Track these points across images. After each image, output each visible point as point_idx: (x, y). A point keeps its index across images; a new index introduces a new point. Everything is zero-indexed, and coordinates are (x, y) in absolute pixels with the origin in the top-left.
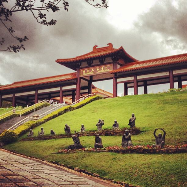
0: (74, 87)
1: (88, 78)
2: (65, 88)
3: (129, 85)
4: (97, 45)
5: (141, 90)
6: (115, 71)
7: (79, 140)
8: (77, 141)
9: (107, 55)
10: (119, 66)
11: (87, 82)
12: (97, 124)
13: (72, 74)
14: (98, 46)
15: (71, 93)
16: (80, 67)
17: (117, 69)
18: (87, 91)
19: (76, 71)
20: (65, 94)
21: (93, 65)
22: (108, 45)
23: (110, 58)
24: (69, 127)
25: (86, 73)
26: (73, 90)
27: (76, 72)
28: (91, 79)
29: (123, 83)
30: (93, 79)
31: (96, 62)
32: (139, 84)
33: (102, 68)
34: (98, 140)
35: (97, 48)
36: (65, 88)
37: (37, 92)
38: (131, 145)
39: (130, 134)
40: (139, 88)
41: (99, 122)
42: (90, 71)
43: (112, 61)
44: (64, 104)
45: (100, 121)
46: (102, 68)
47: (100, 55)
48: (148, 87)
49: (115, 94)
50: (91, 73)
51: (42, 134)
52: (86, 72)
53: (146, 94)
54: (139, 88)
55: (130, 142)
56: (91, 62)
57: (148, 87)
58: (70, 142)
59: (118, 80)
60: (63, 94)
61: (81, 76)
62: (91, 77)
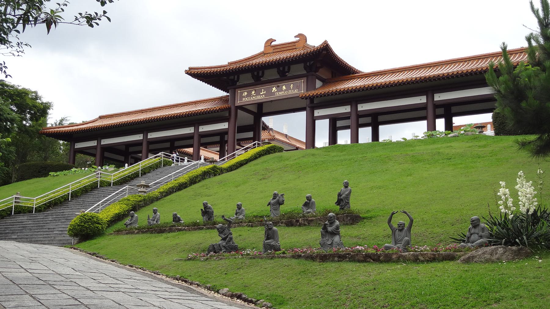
0: (224, 126)
1: (254, 109)
6: (314, 93)
7: (231, 234)
10: (319, 83)
13: (221, 99)
15: (217, 139)
18: (250, 134)
20: (204, 140)
21: (240, 84)
22: (298, 39)
24: (210, 208)
25: (249, 97)
26: (222, 134)
27: (228, 94)
28: (260, 110)
29: (327, 121)
30: (265, 110)
31: (272, 74)
32: (362, 121)
33: (284, 87)
34: (270, 235)
35: (273, 43)
36: (204, 129)
37: (197, 129)
39: (337, 223)
46: (284, 87)
48: (381, 128)
50: (259, 97)
51: (155, 222)
54: (360, 130)
55: (337, 239)
57: (381, 128)
58: (213, 237)
61: (238, 103)
62: (260, 105)
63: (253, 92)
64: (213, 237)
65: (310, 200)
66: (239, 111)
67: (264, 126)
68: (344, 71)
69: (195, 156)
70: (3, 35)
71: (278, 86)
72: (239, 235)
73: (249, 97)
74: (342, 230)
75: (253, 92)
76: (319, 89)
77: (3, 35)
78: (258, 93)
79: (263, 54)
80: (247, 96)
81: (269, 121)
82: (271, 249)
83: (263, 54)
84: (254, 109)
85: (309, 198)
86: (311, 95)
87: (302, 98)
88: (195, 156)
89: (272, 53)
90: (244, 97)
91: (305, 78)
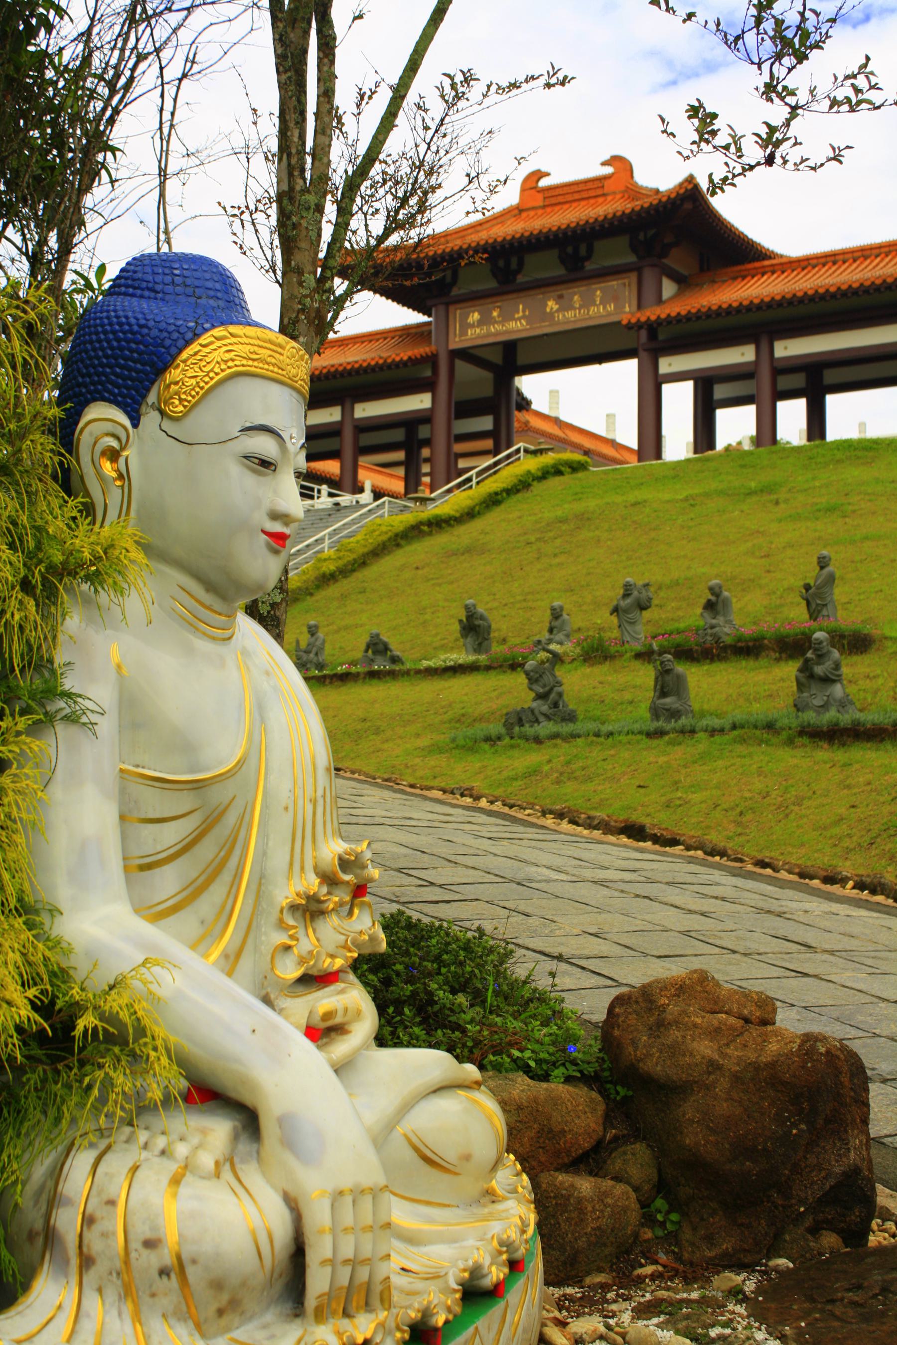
0: (420, 402)
1: (496, 358)
2: (366, 410)
3: (720, 391)
4: (544, 169)
5: (792, 416)
6: (653, 313)
7: (560, 684)
8: (551, 689)
9: (669, 206)
10: (669, 288)
11: (487, 376)
12: (615, 603)
13: (406, 333)
14: (548, 174)
15: (399, 435)
16: (583, 267)
17: (659, 301)
18: (486, 423)
19: (429, 316)
20: (367, 439)
21: (462, 291)
22: (609, 170)
23: (623, 241)
24: (482, 618)
25: (480, 326)
26: (411, 423)
27: (430, 319)
28: (514, 359)
29: (689, 385)
30: (521, 360)
31: (545, 265)
32: (784, 382)
34: (669, 684)
35: (544, 183)
36: (366, 410)
37: (347, 412)
38: (844, 704)
39: (836, 654)
40: (781, 406)
41: (626, 595)
42: (507, 317)
43: (632, 258)
44: (366, 497)
45: (628, 590)
47: (651, 204)
48: (832, 401)
49: (651, 449)
50: (512, 325)
51: (312, 655)
52: (485, 320)
53: (817, 442)
54: (781, 406)
55: (837, 690)
56: (583, 250)
57: (832, 401)
58: (514, 691)
59: (667, 365)
60: (356, 440)
61: (456, 343)
62: (510, 347)
63: (495, 314)
64: (514, 691)
65: (717, 596)
66: (459, 364)
67: (519, 400)
68: (736, 253)
69: (348, 482)
70: (408, 283)
71: (561, 297)
72: (577, 683)
73: (480, 326)
74: (845, 670)
75: (495, 314)
76: (672, 301)
77: (408, 283)
78: (588, 302)
79: (516, 212)
80: (480, 323)
81: (534, 387)
82: (669, 715)
83: (516, 212)
84: (496, 358)
85: (715, 591)
86: (653, 318)
87: (629, 327)
88: (348, 482)
89: (544, 207)
90: (472, 326)
91: (633, 277)
